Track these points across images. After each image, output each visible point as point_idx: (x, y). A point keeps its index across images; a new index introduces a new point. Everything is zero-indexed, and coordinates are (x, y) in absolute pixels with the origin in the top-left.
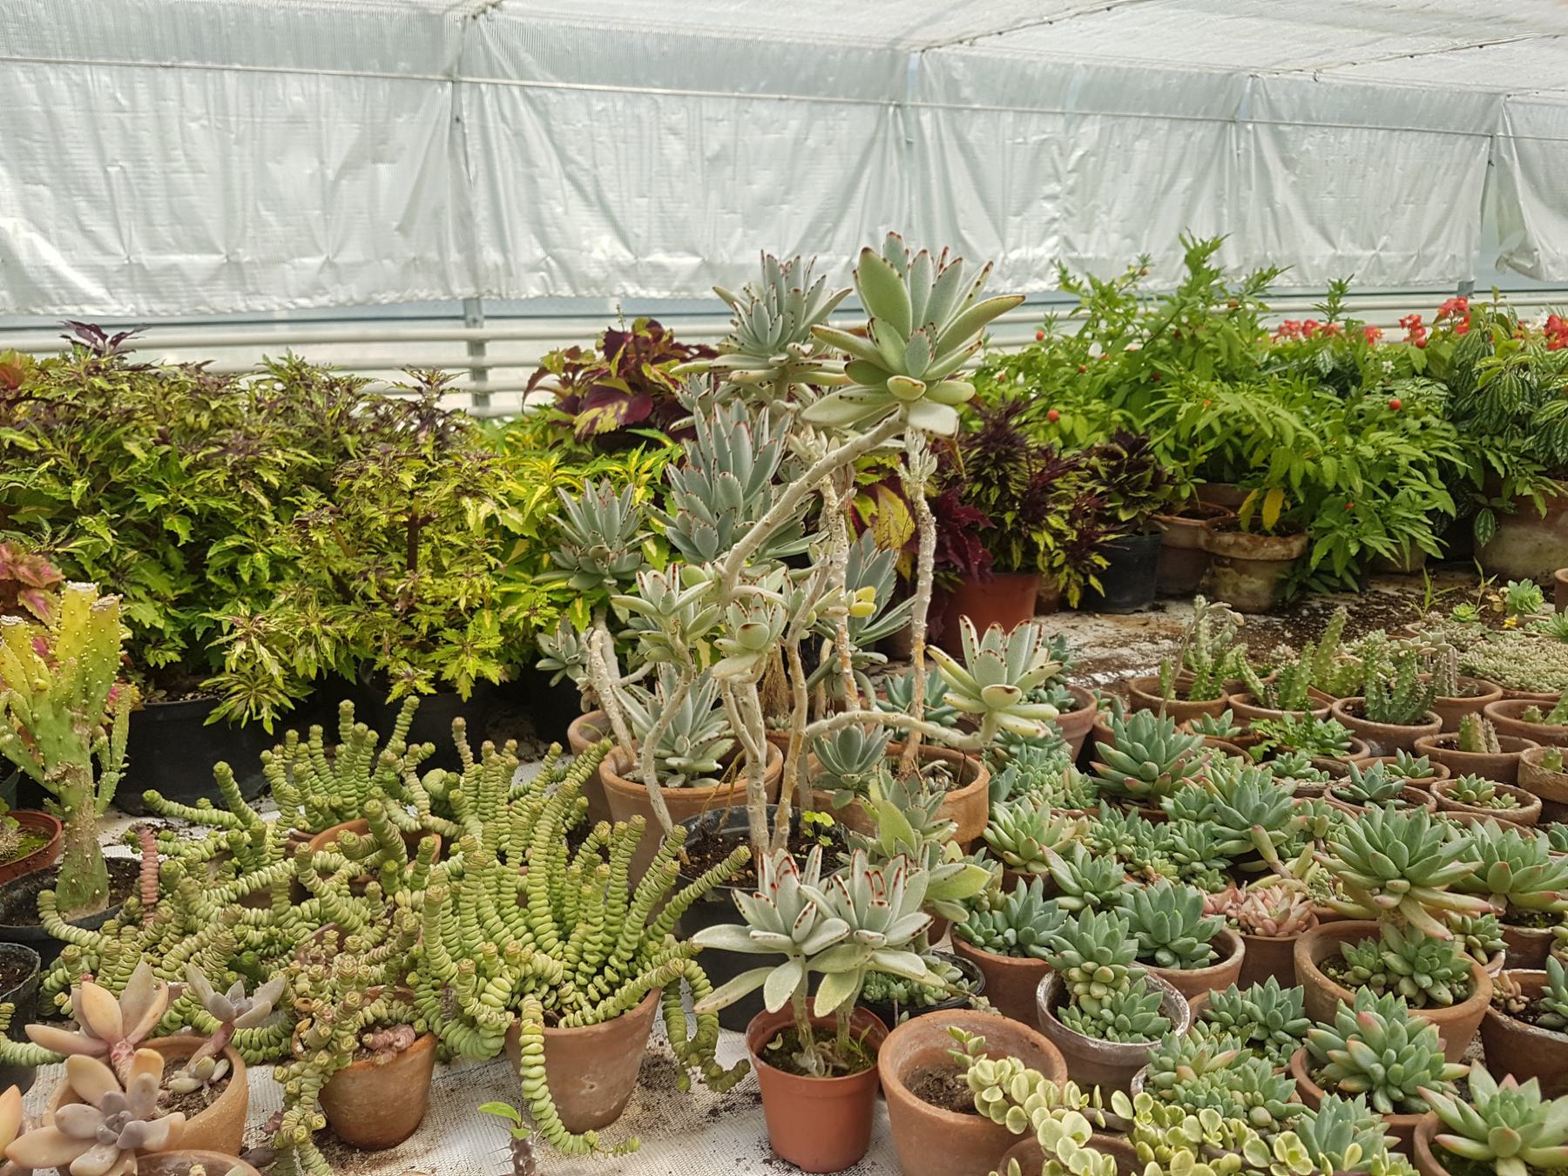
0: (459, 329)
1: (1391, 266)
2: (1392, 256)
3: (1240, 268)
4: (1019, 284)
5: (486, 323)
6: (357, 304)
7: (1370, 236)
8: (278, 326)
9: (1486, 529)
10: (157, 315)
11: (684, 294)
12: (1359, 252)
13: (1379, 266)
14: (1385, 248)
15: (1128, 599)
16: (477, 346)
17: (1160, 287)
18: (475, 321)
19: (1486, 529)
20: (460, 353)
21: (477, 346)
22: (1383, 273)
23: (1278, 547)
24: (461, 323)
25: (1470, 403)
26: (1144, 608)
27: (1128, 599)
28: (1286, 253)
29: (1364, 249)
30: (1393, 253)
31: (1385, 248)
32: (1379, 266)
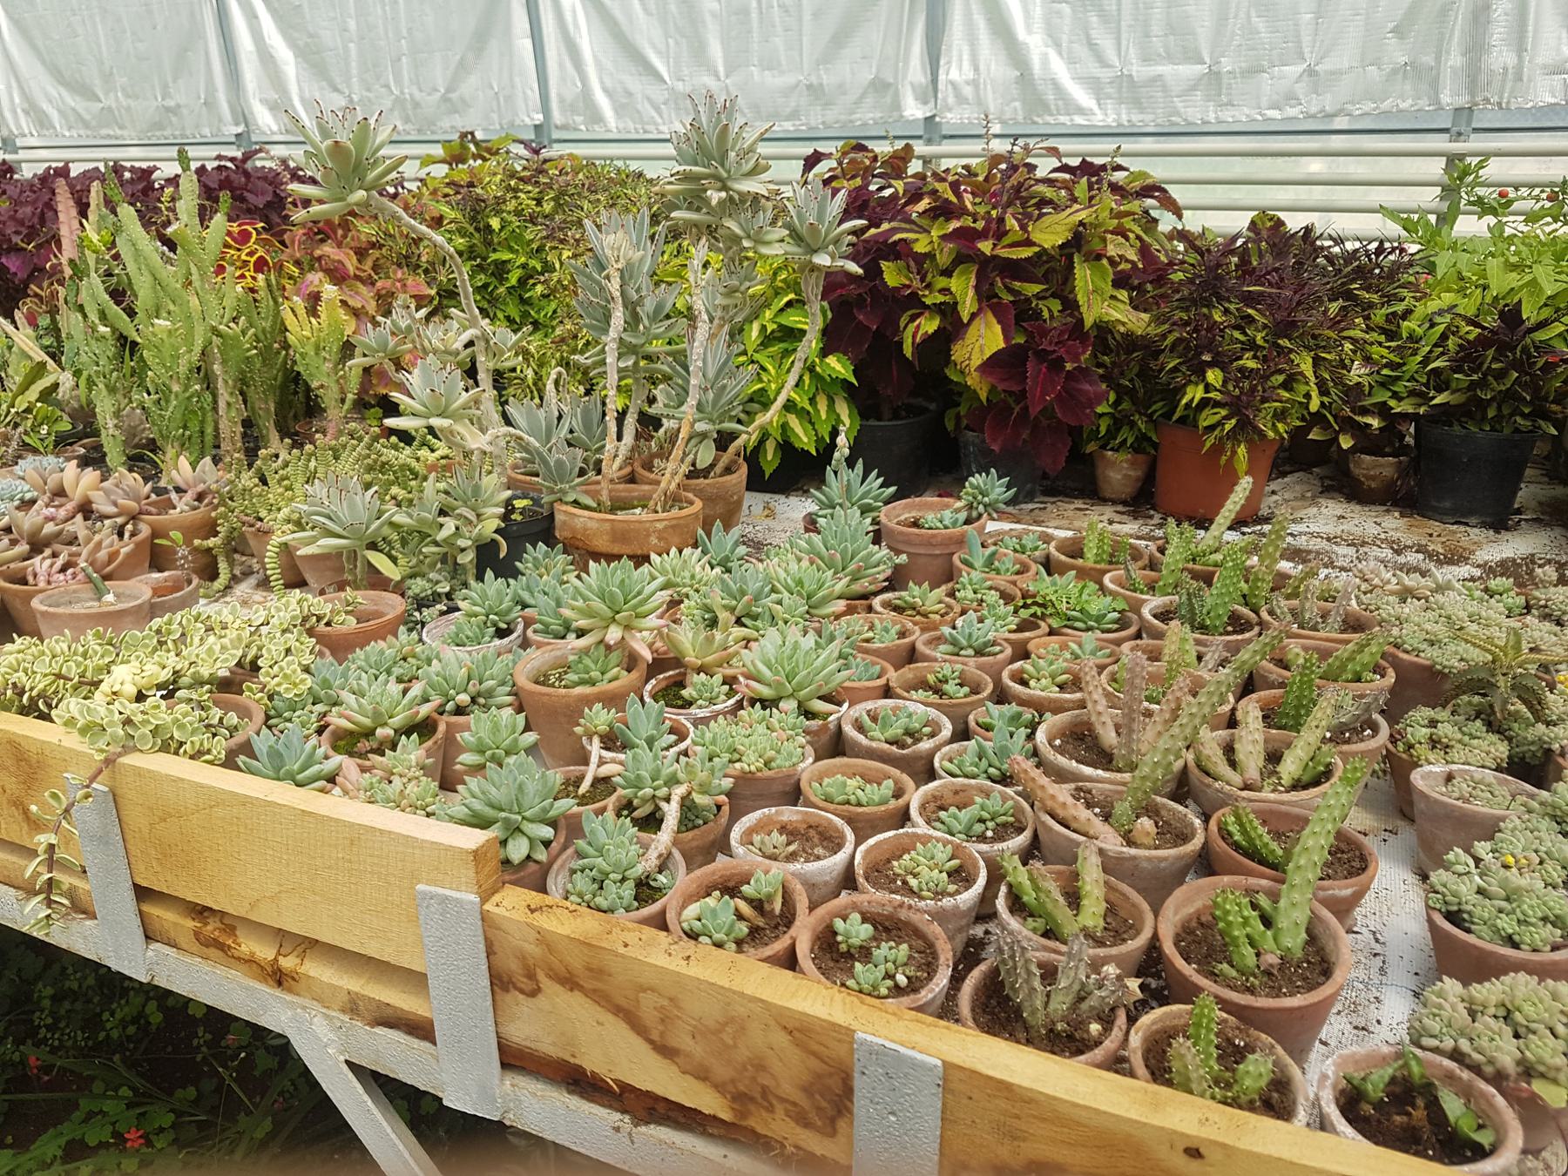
15: (1447, 504)
18: (1460, 134)
26: (1473, 521)
27: (1447, 504)
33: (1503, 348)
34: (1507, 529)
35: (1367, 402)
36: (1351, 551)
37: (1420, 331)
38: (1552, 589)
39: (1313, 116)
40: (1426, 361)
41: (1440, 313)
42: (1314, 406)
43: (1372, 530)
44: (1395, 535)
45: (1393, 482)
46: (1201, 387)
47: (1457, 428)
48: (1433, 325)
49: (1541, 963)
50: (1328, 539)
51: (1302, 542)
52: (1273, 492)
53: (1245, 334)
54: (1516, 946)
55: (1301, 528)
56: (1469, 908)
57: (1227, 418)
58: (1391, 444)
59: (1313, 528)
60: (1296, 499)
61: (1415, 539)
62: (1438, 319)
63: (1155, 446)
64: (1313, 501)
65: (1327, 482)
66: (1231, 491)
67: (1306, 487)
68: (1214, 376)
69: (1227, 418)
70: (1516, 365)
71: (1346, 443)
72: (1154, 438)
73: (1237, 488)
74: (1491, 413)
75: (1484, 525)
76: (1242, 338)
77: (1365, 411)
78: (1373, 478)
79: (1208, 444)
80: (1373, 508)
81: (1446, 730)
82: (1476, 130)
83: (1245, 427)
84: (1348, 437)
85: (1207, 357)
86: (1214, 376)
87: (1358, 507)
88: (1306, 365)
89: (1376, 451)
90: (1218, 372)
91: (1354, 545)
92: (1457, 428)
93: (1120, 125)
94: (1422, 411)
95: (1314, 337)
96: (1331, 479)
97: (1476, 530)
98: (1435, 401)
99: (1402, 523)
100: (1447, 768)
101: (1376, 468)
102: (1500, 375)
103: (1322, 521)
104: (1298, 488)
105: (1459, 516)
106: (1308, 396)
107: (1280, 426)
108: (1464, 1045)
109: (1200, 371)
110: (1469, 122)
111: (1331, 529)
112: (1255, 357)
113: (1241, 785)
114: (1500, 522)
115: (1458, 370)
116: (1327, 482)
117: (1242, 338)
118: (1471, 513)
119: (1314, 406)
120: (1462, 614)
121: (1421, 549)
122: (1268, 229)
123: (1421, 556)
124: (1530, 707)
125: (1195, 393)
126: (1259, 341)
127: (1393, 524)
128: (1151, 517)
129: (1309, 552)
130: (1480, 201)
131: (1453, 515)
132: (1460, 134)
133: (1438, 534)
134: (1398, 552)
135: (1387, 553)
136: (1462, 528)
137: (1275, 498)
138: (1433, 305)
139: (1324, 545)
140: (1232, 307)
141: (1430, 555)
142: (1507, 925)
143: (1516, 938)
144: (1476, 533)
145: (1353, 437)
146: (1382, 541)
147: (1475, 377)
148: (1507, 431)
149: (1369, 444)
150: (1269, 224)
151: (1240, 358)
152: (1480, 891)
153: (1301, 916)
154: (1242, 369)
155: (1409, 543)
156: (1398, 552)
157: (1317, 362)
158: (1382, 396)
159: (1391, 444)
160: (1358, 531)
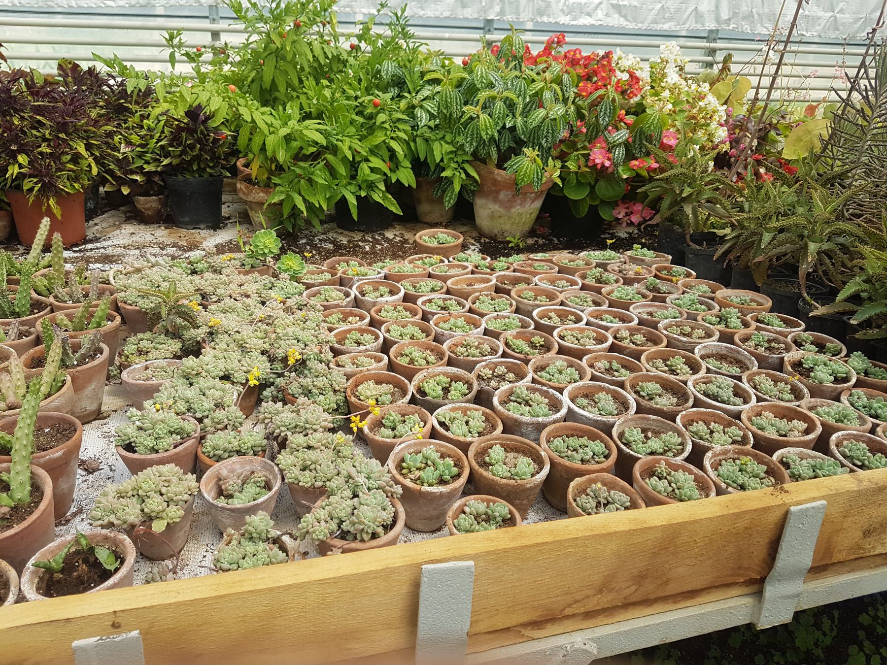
0: (206, 24)
1: (843, 24)
2: (846, 18)
3: (729, 19)
4: (575, 19)
5: (221, 21)
6: (142, 6)
7: (832, 4)
8: (158, 19)
9: (451, 198)
10: (24, 6)
11: (348, 9)
12: (821, 14)
13: (835, 24)
14: (841, 11)
15: (187, 219)
16: (215, 35)
17: (673, 28)
18: (214, 20)
19: (451, 198)
20: (207, 39)
21: (215, 35)
22: (837, 29)
23: (262, 194)
24: (208, 20)
25: (46, 80)
26: (202, 226)
27: (187, 219)
28: (767, 10)
29: (825, 11)
30: (847, 16)
31: (841, 11)
32: (835, 24)
33: (191, 131)
34: (220, 229)
35: (133, 167)
36: (137, 252)
37: (153, 125)
38: (215, 257)
39: (134, 6)
40: (159, 140)
41: (162, 114)
42: (95, 171)
43: (149, 238)
44: (161, 239)
45: (159, 211)
46: (17, 166)
47: (180, 177)
48: (160, 121)
49: (170, 457)
50: (124, 247)
51: (109, 251)
52: (96, 224)
53: (39, 131)
54: (157, 452)
55: (109, 243)
56: (132, 440)
57: (36, 183)
58: (153, 189)
59: (116, 242)
60: (110, 226)
61: (172, 240)
62: (161, 118)
63: (9, 204)
64: (119, 227)
65: (129, 215)
66: (39, 228)
67: (115, 219)
68: (22, 159)
69: (36, 183)
70: (199, 141)
71: (125, 191)
72: (6, 200)
73: (41, 226)
74: (195, 167)
75: (208, 228)
76: (38, 134)
77: (132, 172)
78: (148, 209)
79: (31, 201)
80: (152, 226)
81: (145, 344)
82: (222, 18)
83: (48, 188)
84: (126, 187)
85: (14, 148)
86: (22, 159)
87: (144, 227)
88: (82, 149)
89: (146, 194)
90: (24, 156)
91: (139, 248)
92: (180, 177)
93: (14, 5)
94: (159, 169)
95: (86, 131)
96: (129, 212)
97: (205, 231)
98: (164, 163)
99: (166, 232)
100: (145, 364)
101: (148, 203)
102: (192, 147)
103: (121, 237)
104: (110, 220)
105: (195, 224)
106: (90, 166)
107: (76, 185)
108: (112, 518)
109: (13, 156)
110: (217, 14)
111: (126, 242)
112: (48, 146)
113: (6, 408)
114: (216, 223)
115: (171, 145)
116: (129, 215)
117: (38, 134)
118: (199, 222)
119: (95, 171)
120: (157, 278)
121: (175, 245)
122: (69, 68)
123: (175, 249)
124: (185, 319)
125: (14, 170)
126: (47, 136)
127: (161, 234)
128: (18, 249)
129: (114, 256)
130: (187, 54)
131: (192, 224)
132: (214, 20)
133: (184, 235)
134: (162, 249)
135: (157, 250)
136: (198, 231)
137: (97, 227)
138: (157, 111)
139: (122, 251)
140: (26, 115)
141: (180, 248)
142: (150, 442)
143: (156, 447)
144: (204, 233)
145: (129, 187)
146: (154, 244)
147: (180, 149)
148: (206, 176)
149: (145, 190)
150: (70, 66)
151: (40, 146)
152: (140, 428)
153: (25, 477)
154: (41, 153)
155: (169, 243)
156: (162, 249)
157: (88, 147)
158: (139, 163)
159: (153, 189)
160: (141, 240)
